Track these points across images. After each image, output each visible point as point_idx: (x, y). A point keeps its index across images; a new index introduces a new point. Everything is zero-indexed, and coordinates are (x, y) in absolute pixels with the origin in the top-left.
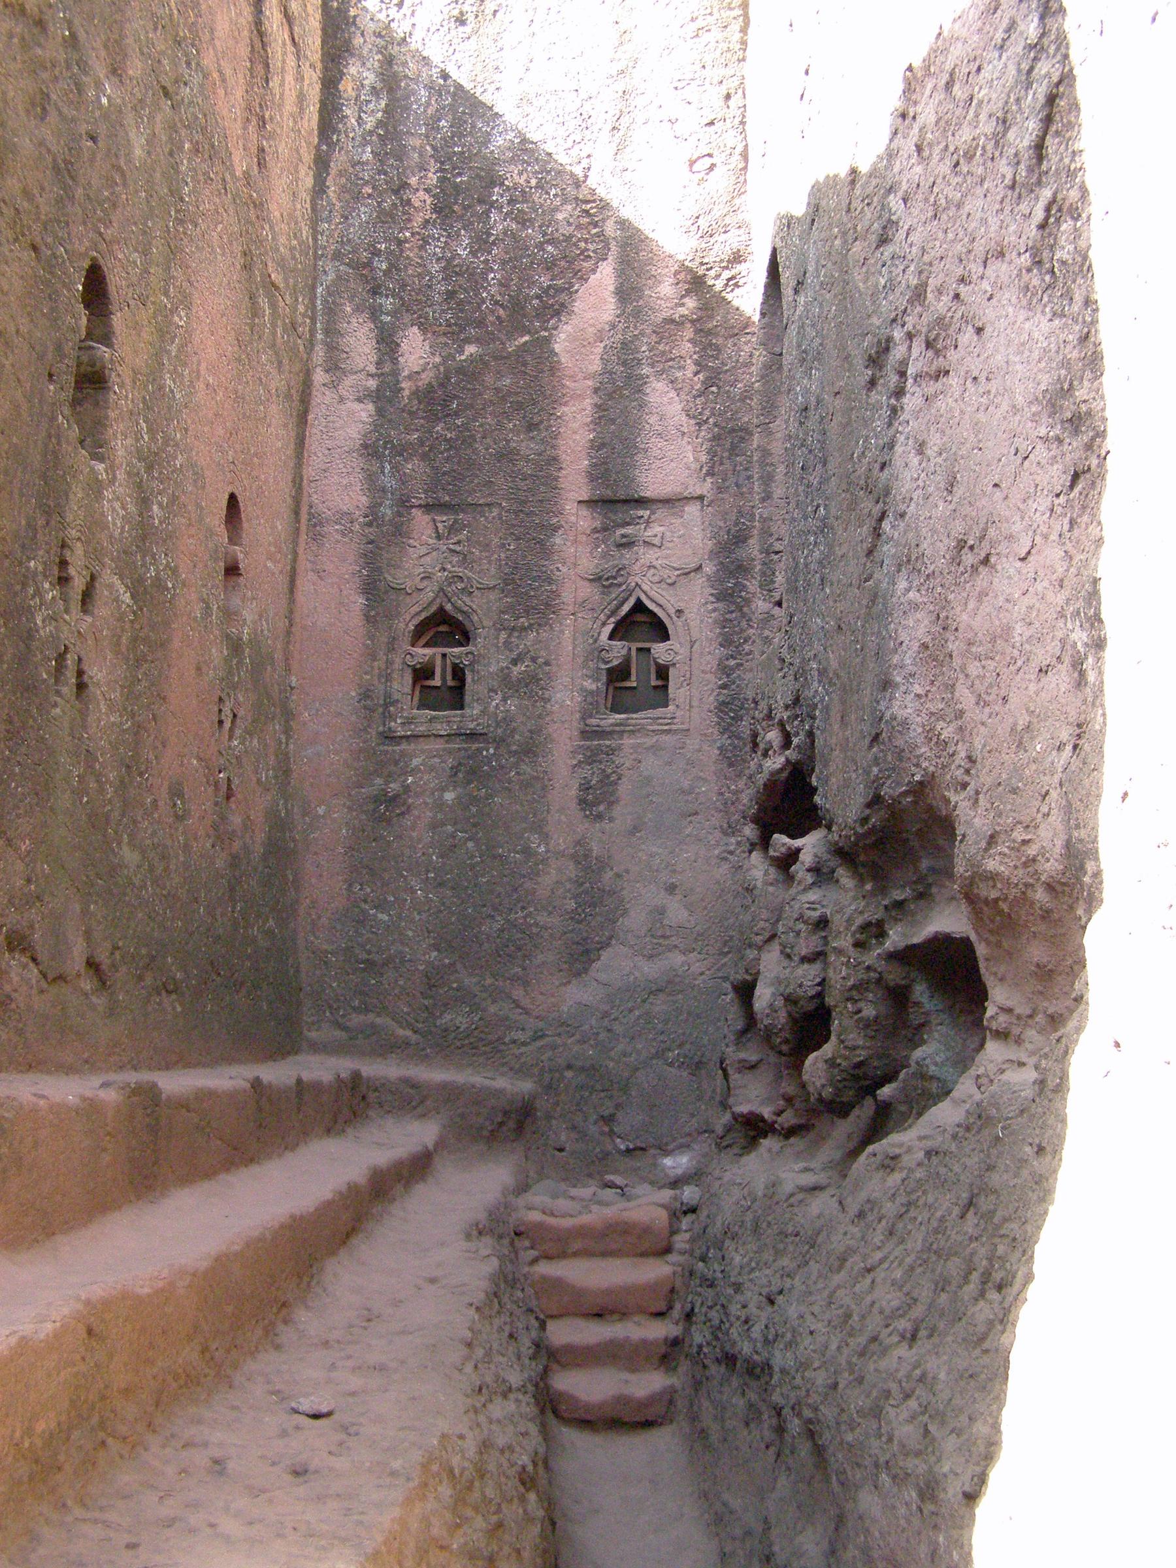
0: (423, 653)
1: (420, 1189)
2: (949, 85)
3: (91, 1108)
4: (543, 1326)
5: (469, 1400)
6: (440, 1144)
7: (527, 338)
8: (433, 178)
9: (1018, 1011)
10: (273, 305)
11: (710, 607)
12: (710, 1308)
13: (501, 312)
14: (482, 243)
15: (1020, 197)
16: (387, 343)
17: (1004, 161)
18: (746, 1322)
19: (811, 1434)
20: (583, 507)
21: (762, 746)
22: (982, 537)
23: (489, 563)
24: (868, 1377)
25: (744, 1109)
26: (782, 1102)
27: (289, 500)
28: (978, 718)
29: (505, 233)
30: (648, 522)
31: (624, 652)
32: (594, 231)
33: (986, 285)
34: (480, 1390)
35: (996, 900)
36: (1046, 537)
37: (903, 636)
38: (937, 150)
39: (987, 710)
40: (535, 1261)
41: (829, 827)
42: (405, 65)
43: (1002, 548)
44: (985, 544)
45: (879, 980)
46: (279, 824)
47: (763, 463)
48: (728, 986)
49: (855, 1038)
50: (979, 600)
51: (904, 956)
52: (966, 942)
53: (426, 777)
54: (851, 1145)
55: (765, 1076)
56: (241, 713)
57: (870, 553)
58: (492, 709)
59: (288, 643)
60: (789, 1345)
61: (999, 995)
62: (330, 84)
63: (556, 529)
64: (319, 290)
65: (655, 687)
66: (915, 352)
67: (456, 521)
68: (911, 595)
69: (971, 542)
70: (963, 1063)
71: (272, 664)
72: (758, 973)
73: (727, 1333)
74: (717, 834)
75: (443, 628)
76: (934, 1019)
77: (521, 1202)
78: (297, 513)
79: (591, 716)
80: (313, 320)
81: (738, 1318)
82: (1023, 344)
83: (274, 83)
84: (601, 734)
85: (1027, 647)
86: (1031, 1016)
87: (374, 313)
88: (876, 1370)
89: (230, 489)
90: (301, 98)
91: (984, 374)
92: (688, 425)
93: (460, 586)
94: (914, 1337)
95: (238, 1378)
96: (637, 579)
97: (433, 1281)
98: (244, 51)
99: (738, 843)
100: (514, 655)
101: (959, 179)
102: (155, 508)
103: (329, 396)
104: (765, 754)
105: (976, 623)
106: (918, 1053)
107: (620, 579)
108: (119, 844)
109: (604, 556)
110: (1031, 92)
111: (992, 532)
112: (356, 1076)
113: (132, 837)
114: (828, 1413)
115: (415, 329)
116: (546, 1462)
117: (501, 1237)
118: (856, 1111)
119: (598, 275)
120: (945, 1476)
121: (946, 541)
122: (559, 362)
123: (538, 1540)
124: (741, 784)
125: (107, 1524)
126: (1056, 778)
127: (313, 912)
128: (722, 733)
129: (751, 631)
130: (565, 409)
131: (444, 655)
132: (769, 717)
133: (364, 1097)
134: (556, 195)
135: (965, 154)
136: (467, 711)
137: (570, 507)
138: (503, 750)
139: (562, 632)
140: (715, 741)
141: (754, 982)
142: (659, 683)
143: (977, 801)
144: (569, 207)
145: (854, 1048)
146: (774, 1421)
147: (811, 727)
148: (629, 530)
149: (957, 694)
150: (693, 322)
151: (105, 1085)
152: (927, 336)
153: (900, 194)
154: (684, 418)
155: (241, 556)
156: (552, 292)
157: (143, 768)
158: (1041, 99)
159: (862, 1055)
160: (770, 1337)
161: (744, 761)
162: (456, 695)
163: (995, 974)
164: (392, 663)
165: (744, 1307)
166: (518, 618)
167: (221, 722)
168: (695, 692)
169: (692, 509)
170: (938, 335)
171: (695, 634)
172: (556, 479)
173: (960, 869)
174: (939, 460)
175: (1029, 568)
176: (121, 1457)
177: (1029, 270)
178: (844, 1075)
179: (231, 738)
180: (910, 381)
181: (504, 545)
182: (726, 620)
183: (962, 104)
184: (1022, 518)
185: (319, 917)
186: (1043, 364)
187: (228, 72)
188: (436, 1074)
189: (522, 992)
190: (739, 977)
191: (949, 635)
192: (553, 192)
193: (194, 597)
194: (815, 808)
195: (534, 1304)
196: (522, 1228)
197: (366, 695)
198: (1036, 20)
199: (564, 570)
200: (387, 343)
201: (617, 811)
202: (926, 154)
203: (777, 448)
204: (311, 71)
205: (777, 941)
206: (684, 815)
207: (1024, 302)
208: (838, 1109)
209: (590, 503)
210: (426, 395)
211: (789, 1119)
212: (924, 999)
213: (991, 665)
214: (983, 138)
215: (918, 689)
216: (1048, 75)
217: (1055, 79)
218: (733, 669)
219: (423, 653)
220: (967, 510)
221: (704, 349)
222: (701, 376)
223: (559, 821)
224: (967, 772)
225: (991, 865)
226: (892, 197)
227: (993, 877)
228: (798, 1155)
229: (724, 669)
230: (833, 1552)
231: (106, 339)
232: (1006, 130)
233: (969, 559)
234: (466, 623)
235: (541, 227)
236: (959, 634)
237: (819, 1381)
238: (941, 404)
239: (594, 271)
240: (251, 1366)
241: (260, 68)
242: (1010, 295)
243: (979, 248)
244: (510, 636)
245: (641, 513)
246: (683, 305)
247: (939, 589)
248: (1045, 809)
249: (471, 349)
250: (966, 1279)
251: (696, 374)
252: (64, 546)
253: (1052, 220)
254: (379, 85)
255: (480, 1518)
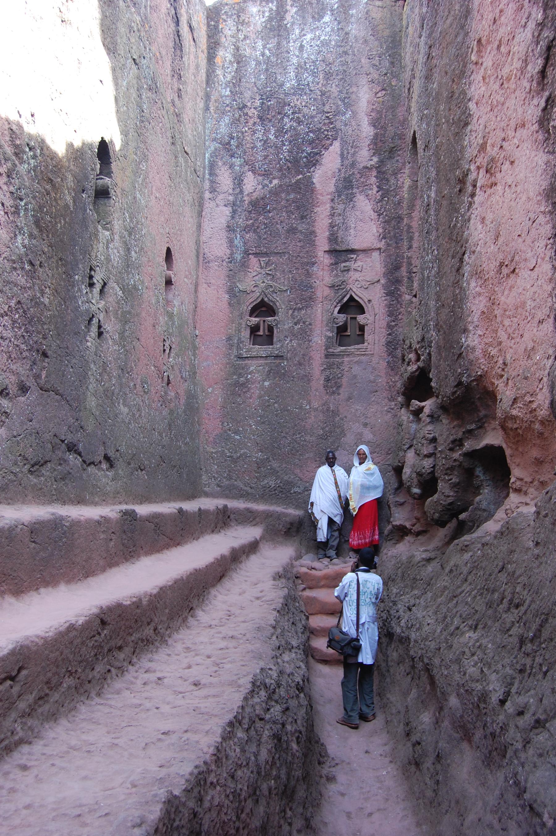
0: (254, 320)
1: (253, 557)
2: (499, 47)
3: (104, 521)
4: (308, 618)
5: (274, 653)
6: (262, 538)
7: (301, 176)
8: (258, 103)
9: (525, 480)
10: (186, 162)
11: (383, 298)
12: (382, 612)
13: (289, 165)
14: (280, 132)
15: (533, 97)
16: (238, 181)
17: (526, 80)
18: (398, 618)
19: (428, 670)
20: (326, 253)
21: (407, 360)
22: (512, 260)
23: (284, 279)
24: (454, 645)
25: (397, 523)
26: (415, 520)
27: (194, 251)
28: (509, 345)
29: (291, 128)
30: (355, 260)
31: (345, 319)
32: (331, 126)
33: (516, 141)
34: (279, 648)
35: (516, 429)
36: (543, 259)
37: (474, 308)
38: (493, 78)
39: (513, 341)
40: (304, 589)
41: (437, 397)
42: (245, 50)
43: (522, 265)
44: (514, 264)
45: (460, 466)
46: (191, 396)
47: (408, 232)
48: (391, 468)
49: (448, 492)
50: (510, 290)
51: (472, 455)
52: (500, 449)
53: (256, 375)
54: (446, 540)
55: (407, 508)
56: (173, 346)
57: (458, 270)
58: (285, 345)
59: (195, 315)
60: (418, 629)
61: (516, 472)
62: (211, 58)
63: (314, 264)
64: (207, 155)
65: (358, 335)
66: (481, 176)
67: (269, 260)
68: (477, 289)
69: (506, 263)
70: (498, 504)
71: (188, 325)
72: (404, 462)
73: (390, 623)
74: (386, 400)
75: (263, 309)
76: (484, 484)
77: (297, 563)
78: (198, 257)
79: (330, 348)
80: (204, 168)
81: (395, 617)
82: (533, 168)
83: (185, 59)
84: (333, 355)
85: (533, 311)
86: (531, 482)
87: (231, 166)
88: (458, 642)
89: (167, 245)
90: (197, 67)
91: (514, 184)
92: (374, 216)
93: (271, 290)
94: (476, 628)
95: (170, 641)
96: (351, 286)
97: (258, 598)
98: (171, 44)
99: (396, 405)
100: (296, 320)
101: (504, 91)
102: (133, 252)
103: (212, 204)
104: (408, 364)
105: (508, 302)
106: (478, 499)
107: (343, 287)
108: (119, 404)
109: (337, 276)
110: (539, 46)
111: (517, 258)
112: (225, 506)
113: (124, 401)
114: (436, 661)
115: (250, 172)
116: (308, 680)
117: (289, 579)
118: (448, 525)
119: (333, 147)
120: (491, 691)
121: (494, 263)
122: (315, 187)
123: (304, 715)
124: (397, 378)
125: (111, 706)
126: (546, 372)
127: (207, 435)
128: (389, 356)
129: (402, 310)
130: (318, 209)
131: (264, 321)
132: (410, 347)
133: (229, 517)
134: (314, 110)
135: (507, 78)
136: (275, 346)
137: (320, 254)
138: (290, 363)
139: (317, 310)
140: (385, 359)
141: (402, 467)
142: (360, 333)
143: (507, 383)
144: (320, 115)
145: (448, 496)
146: (411, 663)
147: (430, 351)
148: (347, 264)
149: (498, 334)
150: (376, 168)
151: (112, 510)
152: (487, 167)
153: (474, 101)
154: (372, 212)
155: (173, 276)
156: (312, 155)
157: (129, 370)
158: (544, 48)
159: (450, 500)
160: (409, 626)
161: (398, 368)
162: (269, 339)
163: (515, 463)
164: (241, 324)
165: (397, 611)
166: (297, 304)
167: (164, 350)
168: (377, 337)
169: (376, 254)
170: (492, 166)
171: (377, 311)
172: (314, 241)
173: (499, 414)
174: (492, 225)
175: (534, 274)
176: (117, 676)
177: (537, 132)
178: (444, 508)
179: (169, 357)
180: (478, 189)
181: (290, 271)
182: (391, 304)
183: (505, 55)
184: (532, 251)
185: (209, 437)
186: (544, 176)
187: (164, 53)
188: (260, 507)
189: (299, 471)
190: (396, 464)
191: (495, 307)
192: (312, 108)
193: (151, 293)
194: (431, 388)
195: (303, 609)
196: (298, 575)
197: (229, 339)
198: (542, 11)
199: (318, 282)
200: (238, 181)
201: (341, 391)
202: (487, 80)
203: (415, 224)
204: (202, 54)
205: (413, 448)
206: (372, 392)
207: (535, 148)
208: (442, 524)
209: (330, 252)
210: (255, 204)
211: (417, 528)
212: (481, 475)
213: (515, 320)
214: (515, 70)
215: (480, 332)
216: (548, 37)
217: (551, 38)
218: (393, 327)
219: (254, 320)
220: (505, 248)
221: (382, 180)
222: (380, 193)
223: (315, 395)
224: (503, 370)
225: (514, 412)
226: (470, 103)
227: (514, 418)
228: (422, 544)
229: (389, 326)
230: (437, 723)
231: (109, 174)
232: (527, 66)
233: (505, 271)
234: (275, 307)
235: (307, 124)
236: (500, 306)
237: (432, 646)
238: (494, 199)
239: (331, 145)
240: (176, 636)
241: (178, 52)
242: (526, 145)
243: (513, 124)
244: (293, 312)
245: (352, 256)
246: (372, 160)
247: (491, 286)
248: (541, 386)
249: (275, 182)
250: (501, 602)
251: (378, 192)
252: (91, 269)
253: (549, 107)
254: (232, 60)
255: (279, 706)
